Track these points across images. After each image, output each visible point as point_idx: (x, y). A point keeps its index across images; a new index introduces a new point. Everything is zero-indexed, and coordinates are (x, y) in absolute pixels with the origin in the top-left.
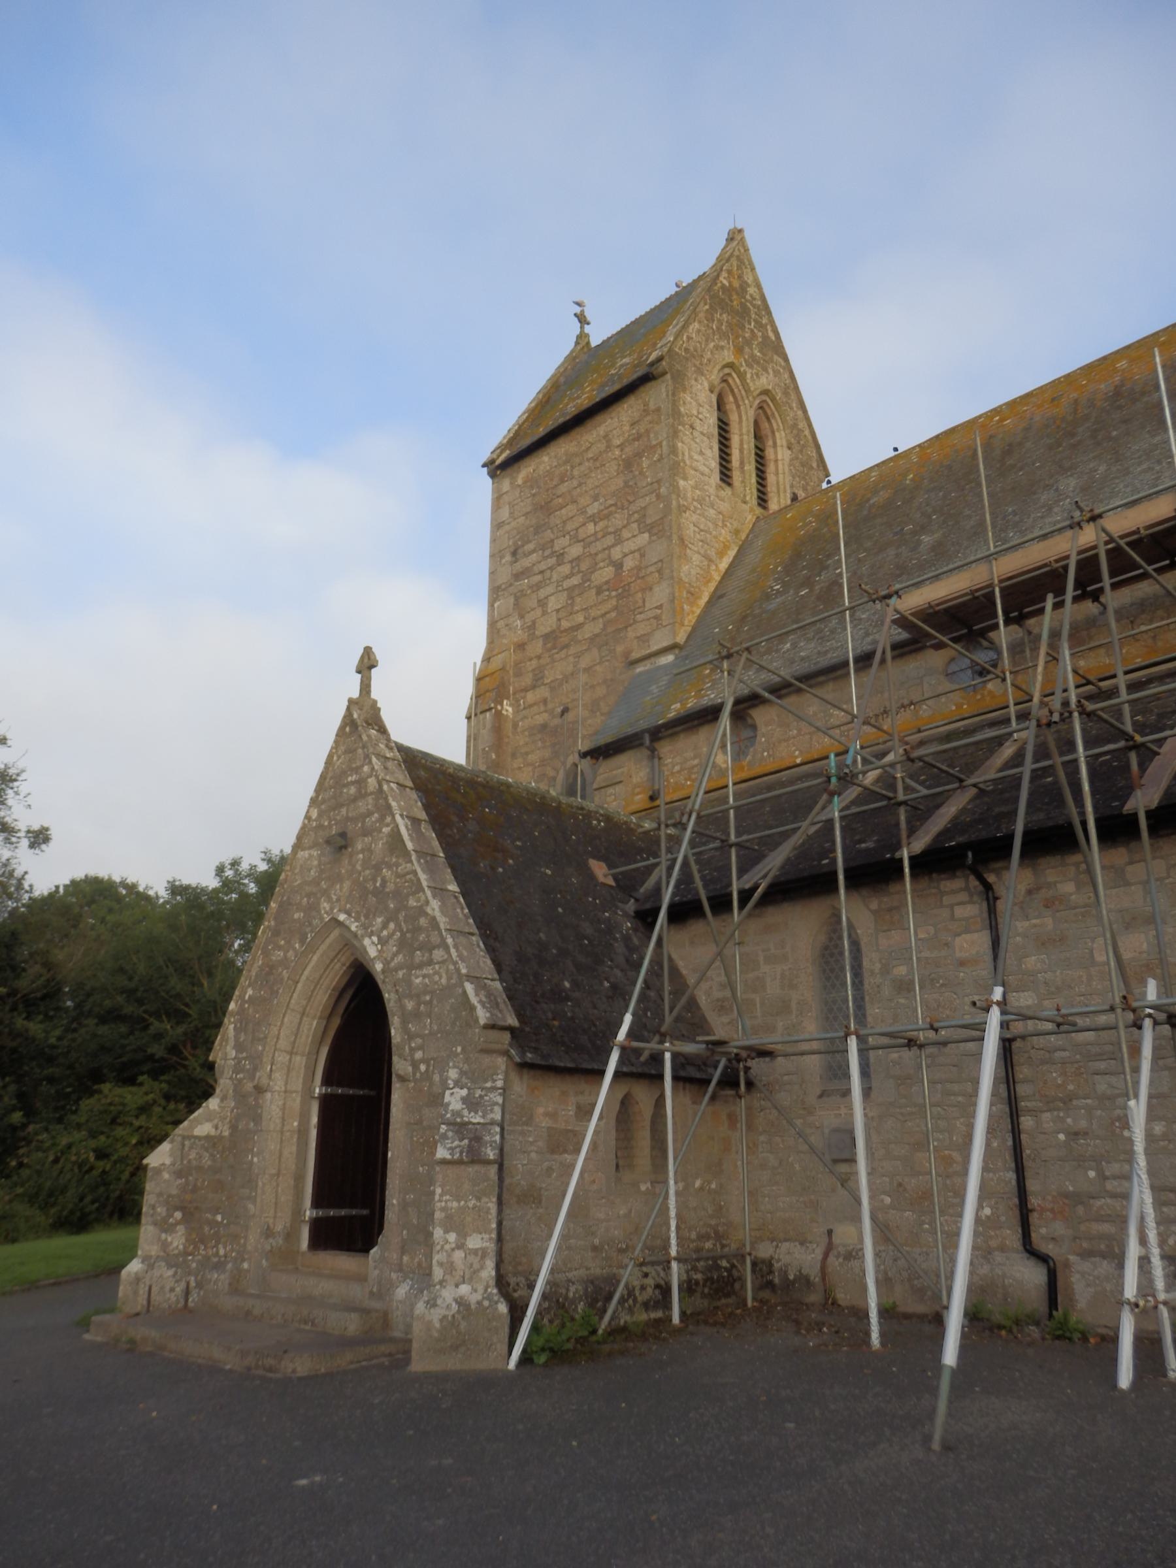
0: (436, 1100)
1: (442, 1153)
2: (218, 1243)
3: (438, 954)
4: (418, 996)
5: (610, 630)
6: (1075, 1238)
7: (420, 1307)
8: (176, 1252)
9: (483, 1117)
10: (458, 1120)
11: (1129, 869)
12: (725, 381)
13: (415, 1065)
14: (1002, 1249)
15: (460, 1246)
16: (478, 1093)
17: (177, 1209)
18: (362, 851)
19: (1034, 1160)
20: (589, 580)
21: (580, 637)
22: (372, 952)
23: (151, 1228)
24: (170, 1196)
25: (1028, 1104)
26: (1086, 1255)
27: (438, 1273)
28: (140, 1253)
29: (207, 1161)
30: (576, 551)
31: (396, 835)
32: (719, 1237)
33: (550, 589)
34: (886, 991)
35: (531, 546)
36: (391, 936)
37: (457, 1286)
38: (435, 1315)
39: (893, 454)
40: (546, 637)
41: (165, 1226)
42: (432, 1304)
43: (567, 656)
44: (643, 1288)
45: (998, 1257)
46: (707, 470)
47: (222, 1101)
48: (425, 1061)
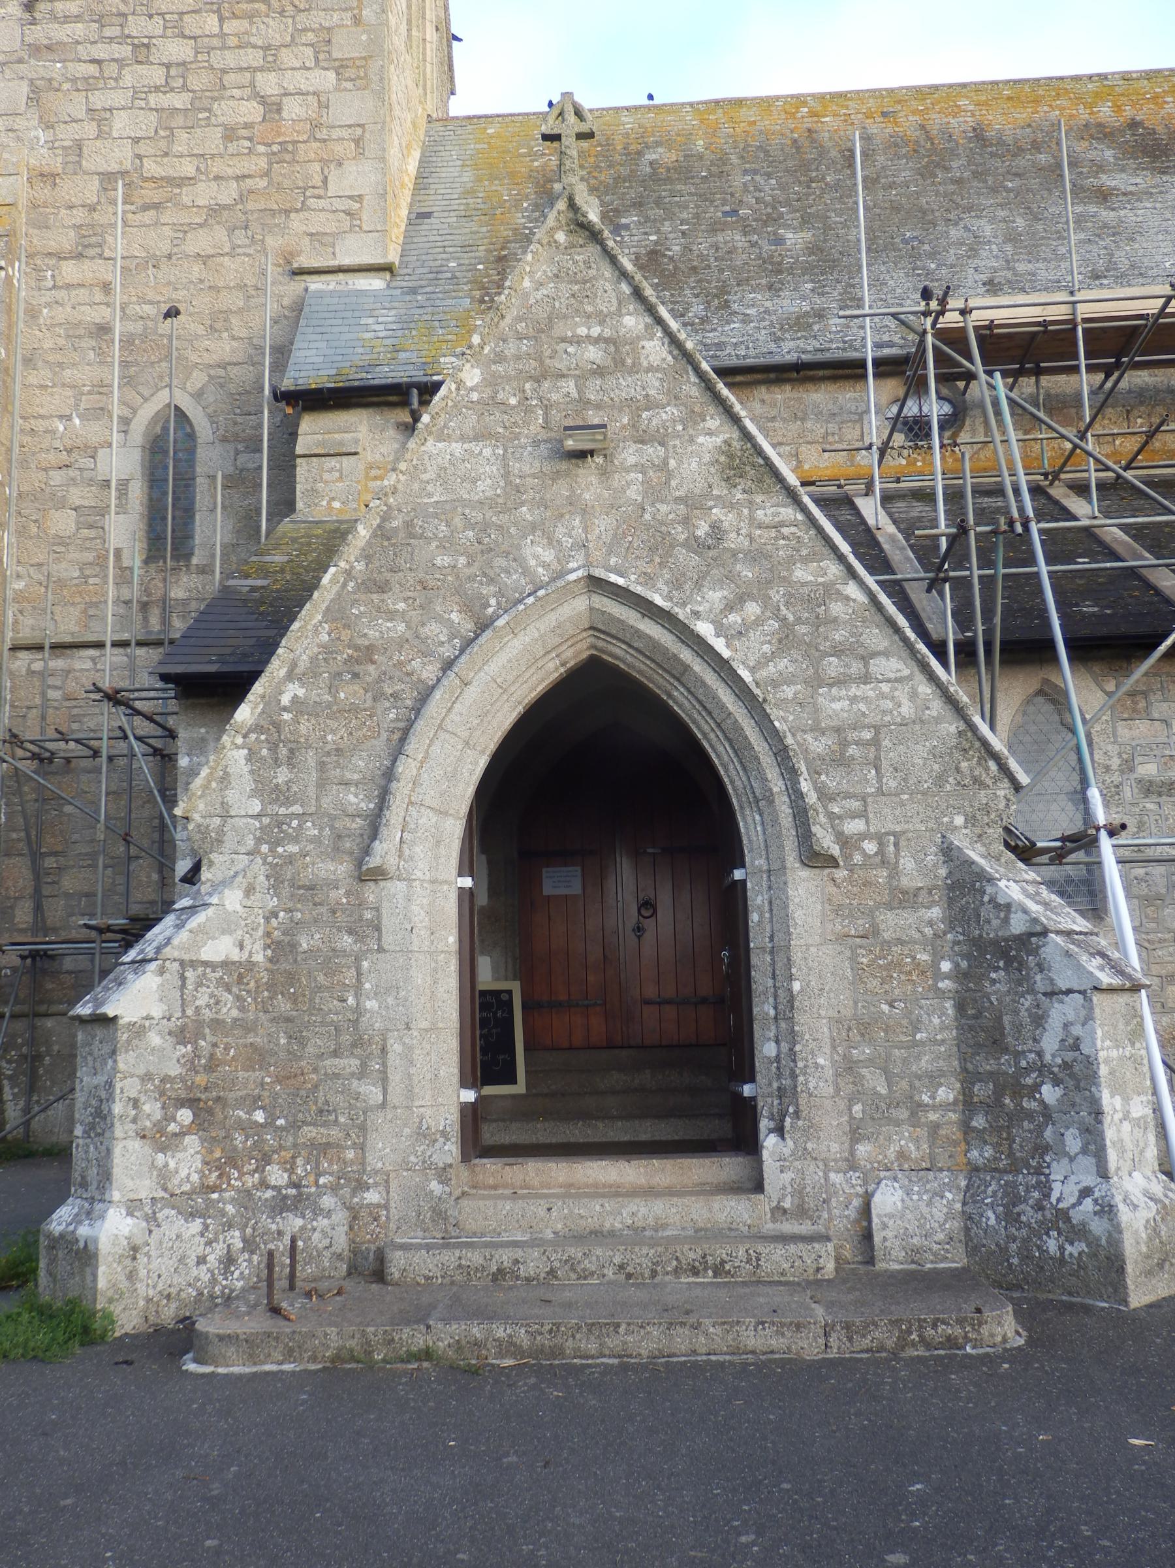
8: (187, 1187)
17: (181, 1103)
21: (186, 200)
23: (136, 1145)
28: (116, 1195)
29: (228, 1010)
33: (118, 98)
39: (646, 102)
40: (108, 179)
41: (162, 1139)
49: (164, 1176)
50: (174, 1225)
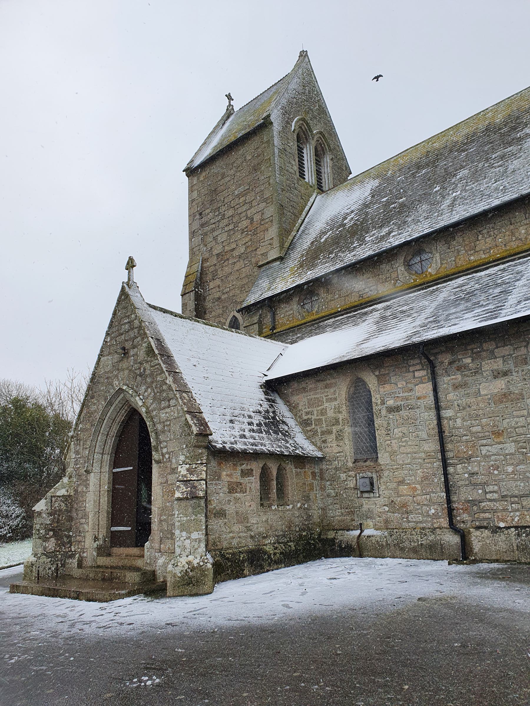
0: (174, 471)
1: (178, 495)
2: (71, 545)
3: (172, 402)
4: (164, 422)
5: (248, 250)
6: (472, 521)
7: (170, 567)
9: (197, 477)
10: (185, 479)
11: (496, 350)
12: (301, 127)
13: (163, 455)
14: (440, 528)
15: (188, 538)
16: (194, 466)
17: (51, 530)
18: (133, 355)
19: (454, 487)
20: (237, 226)
22: (140, 403)
24: (47, 524)
25: (451, 461)
26: (478, 528)
27: (178, 551)
30: (231, 212)
31: (150, 347)
32: (309, 529)
33: (220, 231)
34: (384, 412)
35: (208, 211)
36: (149, 395)
37: (187, 556)
38: (178, 571)
40: (218, 255)
42: (175, 565)
43: (228, 264)
44: (275, 554)
45: (438, 531)
46: (293, 172)
47: (69, 478)
48: (167, 453)
49: (45, 548)
50: (44, 559)
